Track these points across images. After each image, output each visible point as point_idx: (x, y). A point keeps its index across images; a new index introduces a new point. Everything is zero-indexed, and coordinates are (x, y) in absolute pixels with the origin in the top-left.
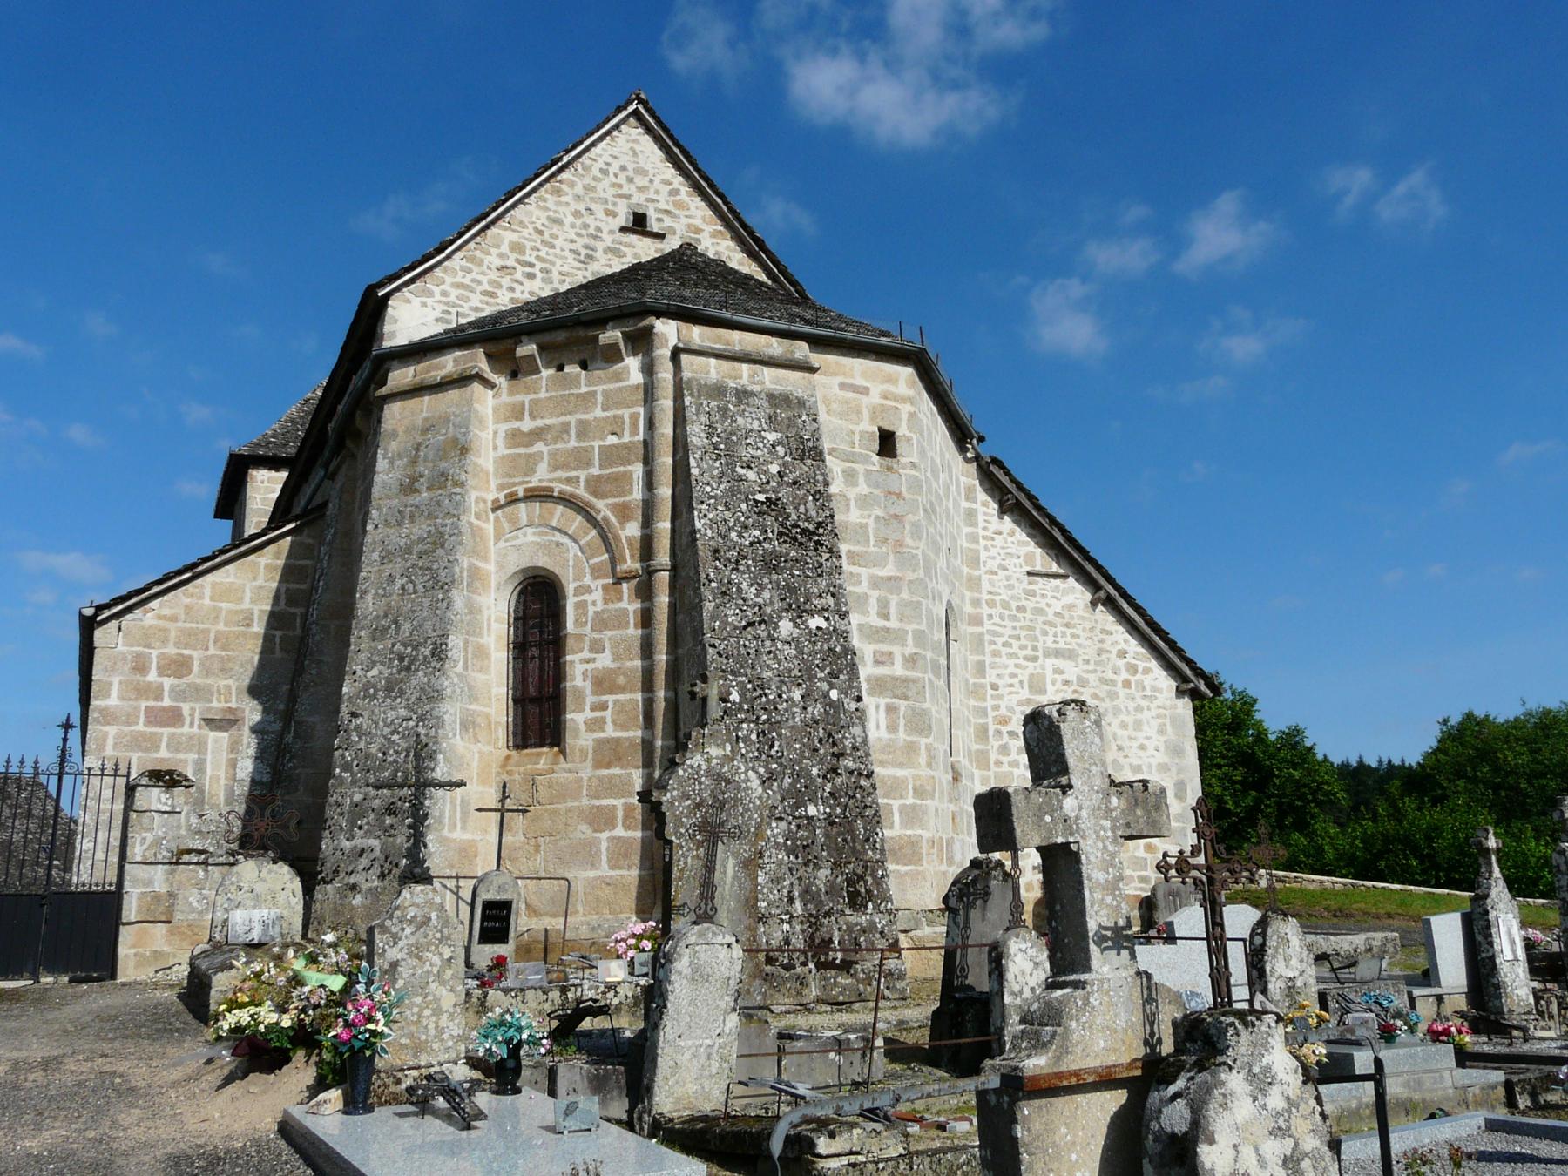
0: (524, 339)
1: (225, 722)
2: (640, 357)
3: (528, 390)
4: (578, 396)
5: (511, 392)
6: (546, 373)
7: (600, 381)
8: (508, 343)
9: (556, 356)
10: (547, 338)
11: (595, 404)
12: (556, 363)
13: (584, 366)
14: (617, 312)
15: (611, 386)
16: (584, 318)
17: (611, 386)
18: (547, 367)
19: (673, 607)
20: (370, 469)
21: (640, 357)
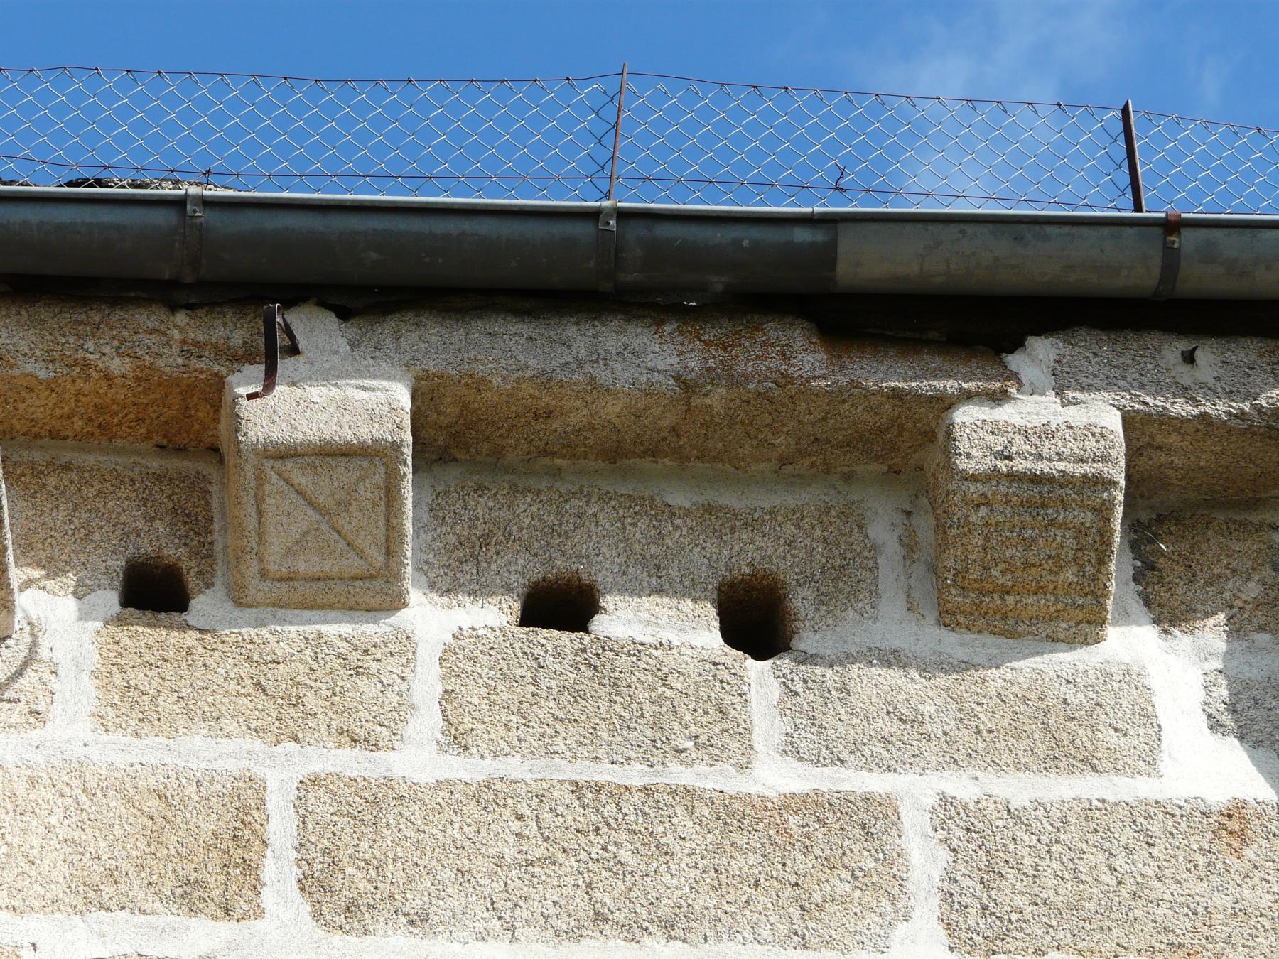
0: (313, 327)
1: (1189, 358)
2: (1212, 634)
3: (288, 716)
4: (734, 814)
5: (128, 704)
6: (445, 624)
7: (903, 740)
8: (157, 343)
9: (528, 510)
10: (504, 356)
11: (892, 890)
12: (526, 569)
13: (756, 623)
14: (1137, 272)
15: (1019, 789)
16: (862, 265)
17: (1019, 789)
18: (458, 573)
19: (235, 189)
20: (1025, 657)
21: (1212, 634)
